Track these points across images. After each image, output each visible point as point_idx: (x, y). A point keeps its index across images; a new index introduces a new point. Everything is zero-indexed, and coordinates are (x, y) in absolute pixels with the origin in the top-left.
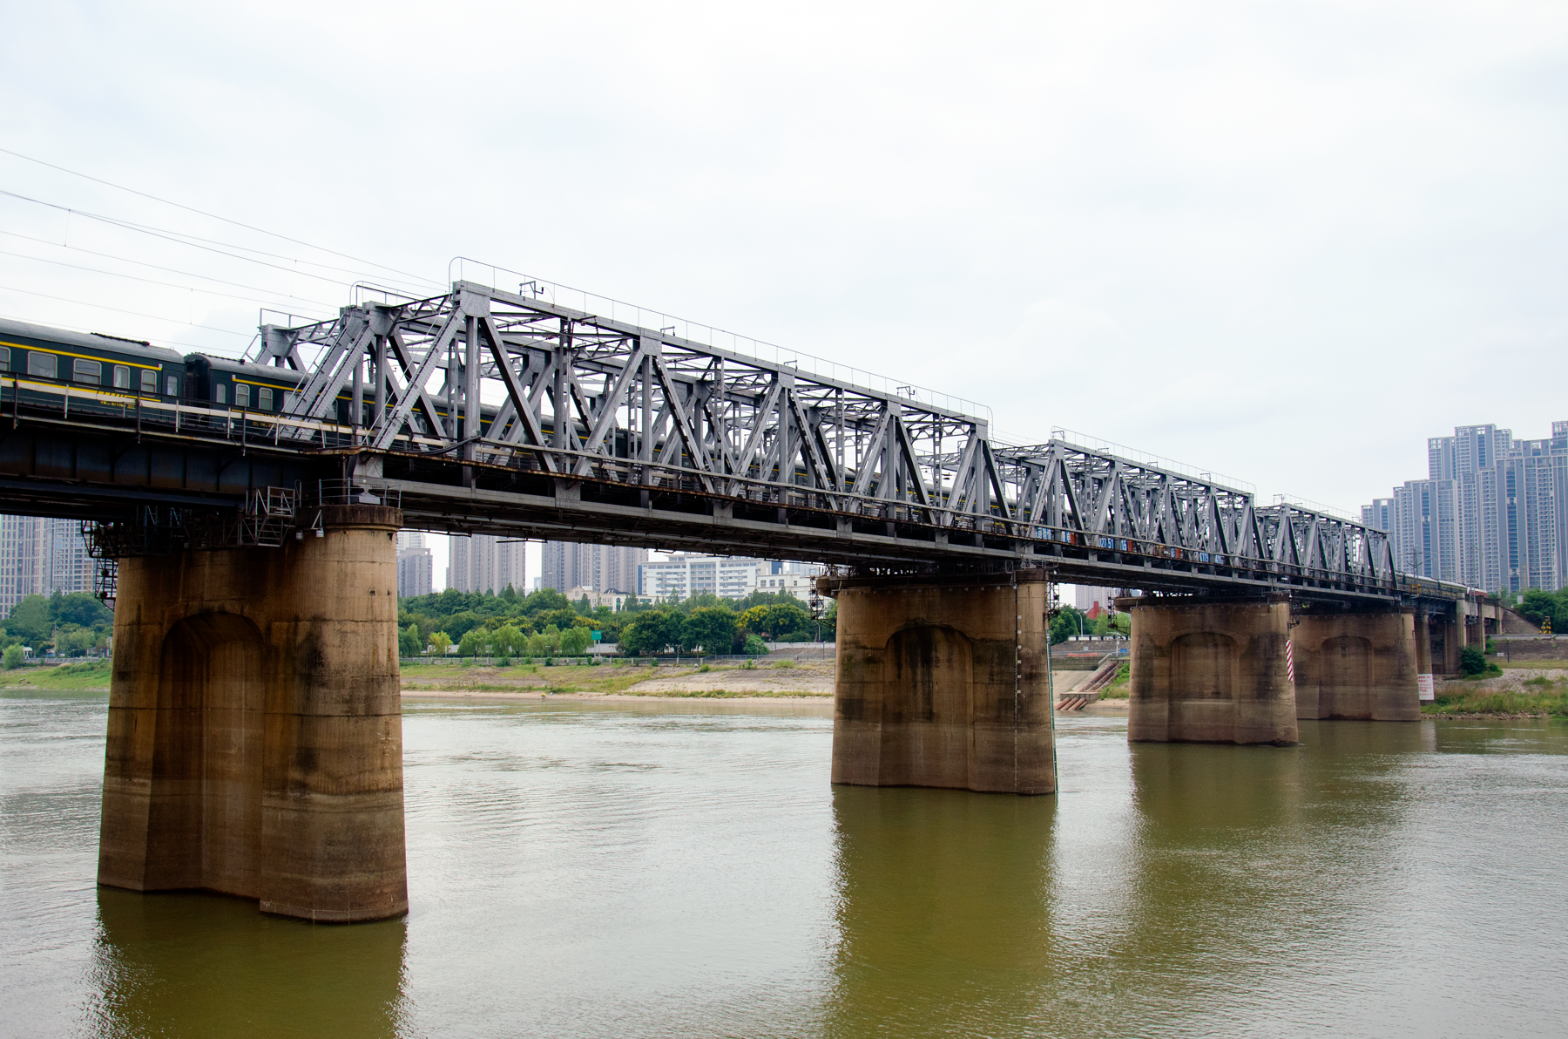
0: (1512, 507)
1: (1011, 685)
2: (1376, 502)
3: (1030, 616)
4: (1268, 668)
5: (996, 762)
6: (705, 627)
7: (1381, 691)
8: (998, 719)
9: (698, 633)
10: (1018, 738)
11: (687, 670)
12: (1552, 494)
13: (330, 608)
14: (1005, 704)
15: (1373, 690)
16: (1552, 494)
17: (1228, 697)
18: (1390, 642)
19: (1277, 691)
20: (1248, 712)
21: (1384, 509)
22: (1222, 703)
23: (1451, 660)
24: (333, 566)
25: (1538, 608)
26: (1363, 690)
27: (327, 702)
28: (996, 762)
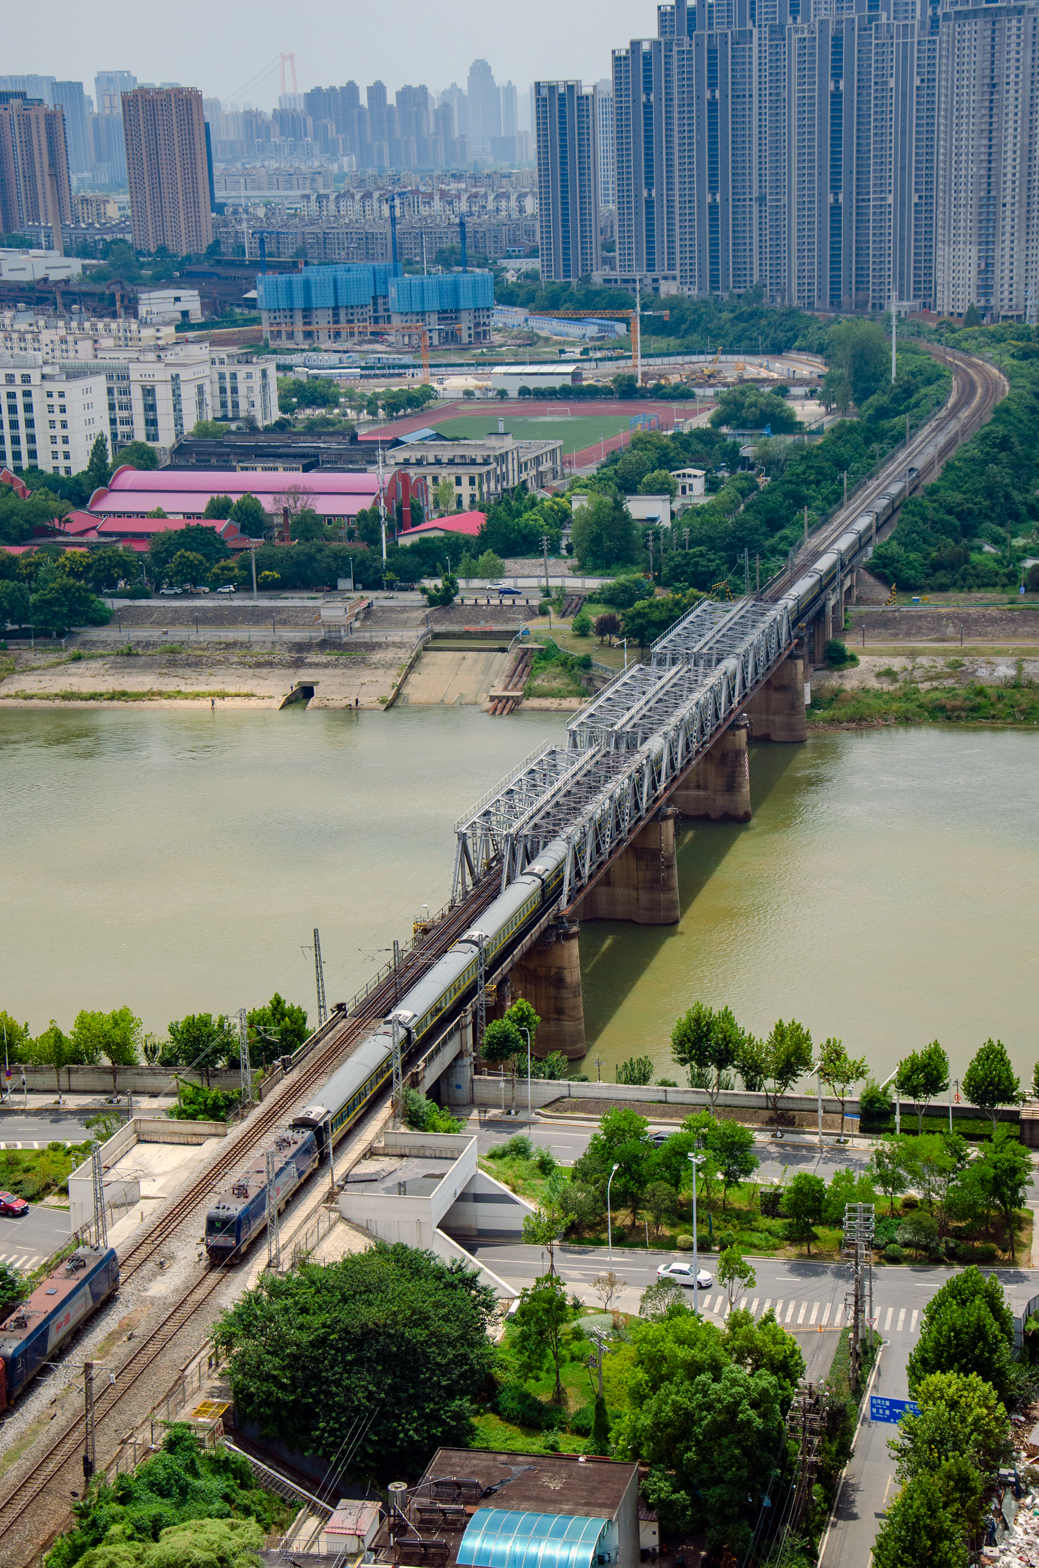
0: (836, 95)
1: (659, 871)
2: (635, 45)
3: (667, 837)
4: (734, 772)
5: (651, 909)
6: (62, 605)
7: (778, 719)
8: (651, 888)
9: (56, 613)
10: (663, 897)
11: (52, 658)
12: (892, 83)
13: (566, 965)
14: (656, 880)
15: (772, 718)
16: (890, 200)
17: (706, 789)
18: (786, 682)
19: (740, 786)
20: (721, 801)
21: (647, 57)
22: (701, 793)
23: (819, 652)
24: (566, 951)
25: (885, 566)
26: (764, 717)
27: (566, 993)
28: (651, 909)
